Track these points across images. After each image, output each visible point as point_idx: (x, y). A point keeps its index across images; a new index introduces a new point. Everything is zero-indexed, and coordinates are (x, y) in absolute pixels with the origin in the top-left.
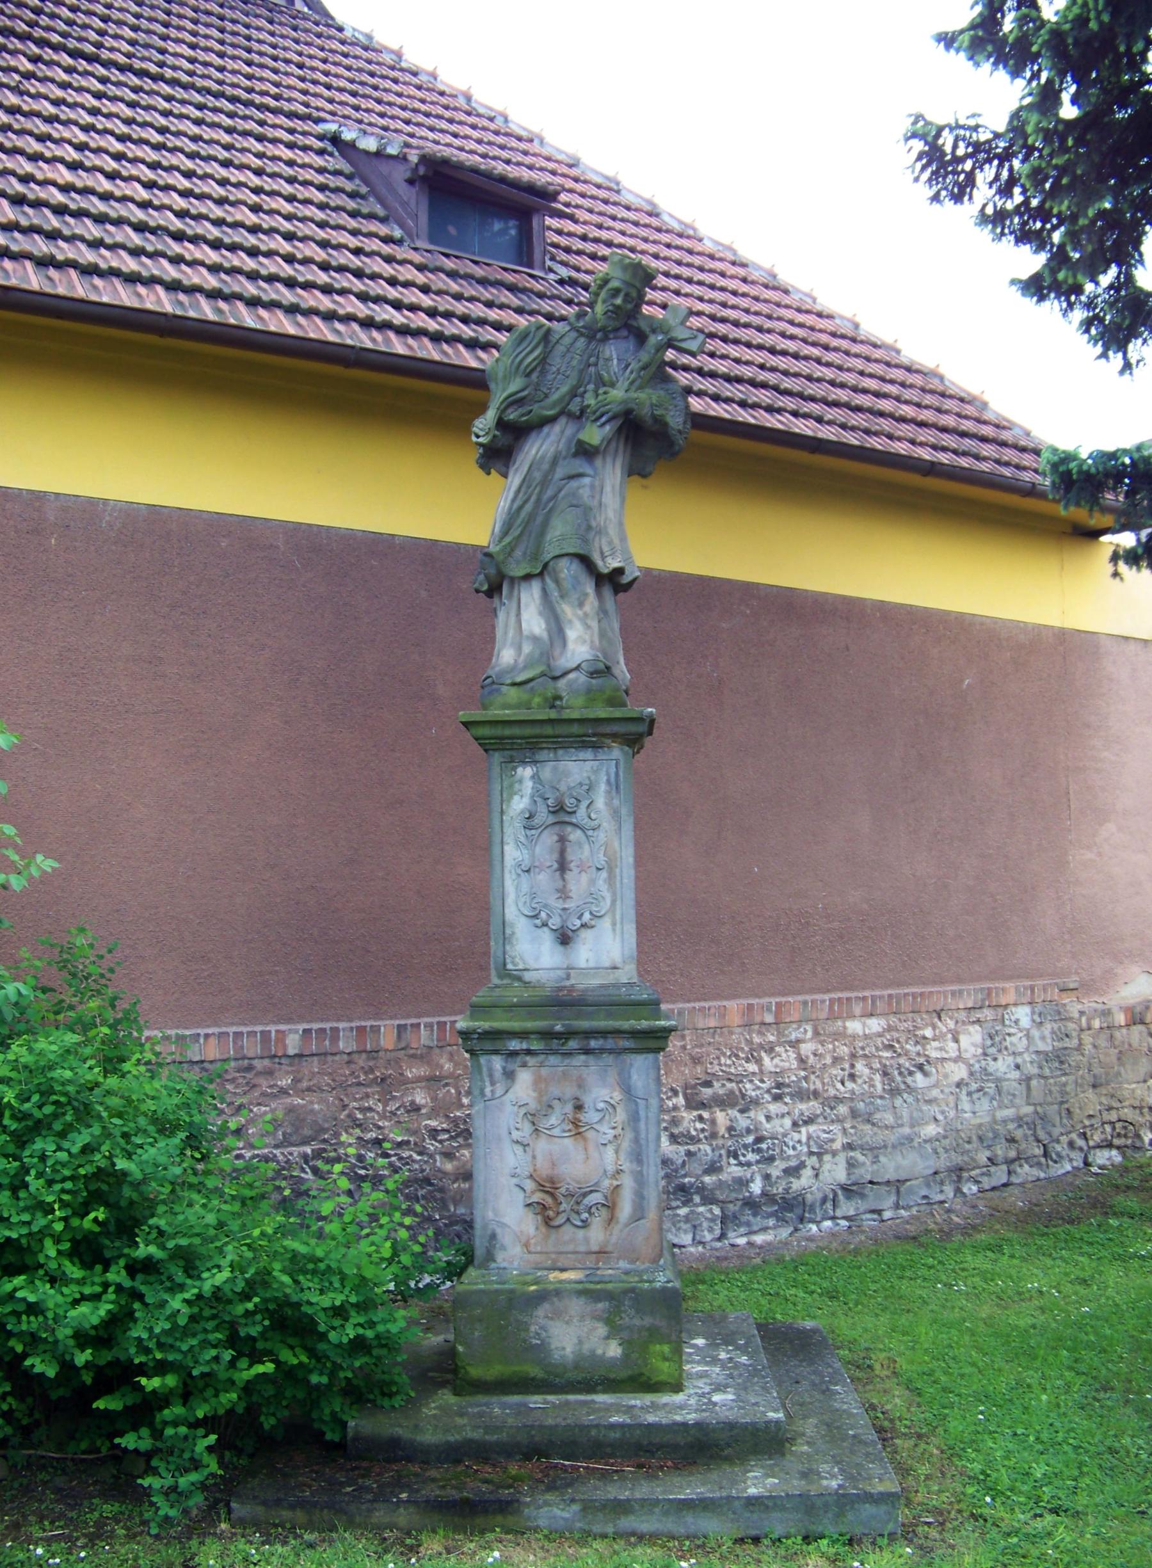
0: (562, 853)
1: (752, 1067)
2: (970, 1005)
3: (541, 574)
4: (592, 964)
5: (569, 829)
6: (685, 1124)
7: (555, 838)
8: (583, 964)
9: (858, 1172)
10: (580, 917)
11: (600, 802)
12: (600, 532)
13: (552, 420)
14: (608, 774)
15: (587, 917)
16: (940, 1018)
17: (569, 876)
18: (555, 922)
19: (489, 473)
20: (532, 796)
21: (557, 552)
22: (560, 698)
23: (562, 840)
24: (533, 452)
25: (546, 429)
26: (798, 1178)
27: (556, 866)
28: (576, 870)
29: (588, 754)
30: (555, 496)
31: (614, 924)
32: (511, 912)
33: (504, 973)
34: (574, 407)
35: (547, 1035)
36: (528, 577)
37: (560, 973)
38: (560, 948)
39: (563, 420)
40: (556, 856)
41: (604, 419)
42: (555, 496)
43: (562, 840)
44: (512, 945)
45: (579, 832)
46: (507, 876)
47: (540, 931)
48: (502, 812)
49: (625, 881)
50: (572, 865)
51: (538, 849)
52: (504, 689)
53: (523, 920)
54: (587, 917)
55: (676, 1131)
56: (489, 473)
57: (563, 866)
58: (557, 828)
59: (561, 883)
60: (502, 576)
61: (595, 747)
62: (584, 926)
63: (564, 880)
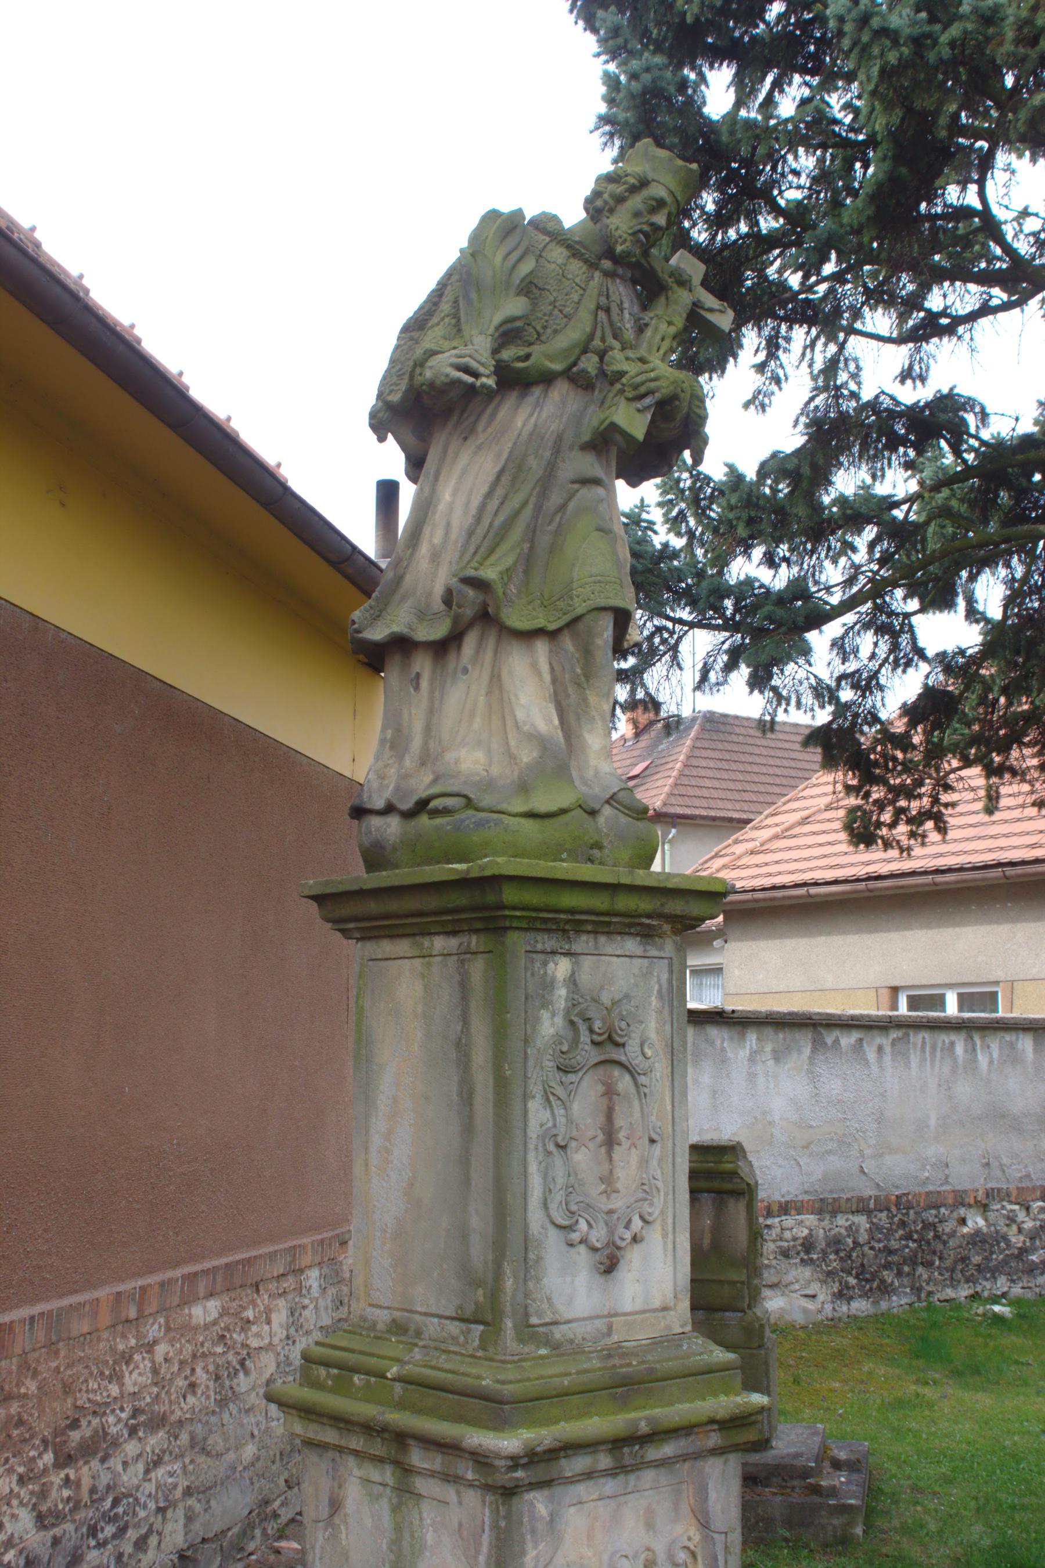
0: (610, 1115)
1: (114, 1390)
2: (281, 1271)
3: (552, 635)
4: (639, 1306)
5: (617, 1072)
6: (54, 1494)
7: (601, 1088)
8: (628, 1308)
9: (196, 1526)
10: (627, 1226)
11: (653, 1025)
12: (976, 602)
13: (547, 379)
14: (659, 981)
15: (637, 1224)
16: (258, 1291)
17: (618, 1152)
18: (598, 1236)
19: (382, 439)
20: (567, 1012)
21: (603, 602)
22: (599, 846)
23: (610, 1092)
24: (519, 424)
25: (537, 391)
26: (146, 1551)
27: (601, 1137)
28: (626, 1144)
29: (631, 945)
30: (563, 507)
31: (665, 1236)
32: (536, 1217)
33: (527, 1332)
34: (589, 364)
35: (617, 1443)
36: (529, 636)
37: (599, 1324)
38: (600, 1280)
39: (561, 389)
40: (601, 1118)
41: (648, 401)
42: (563, 507)
43: (610, 1092)
44: (538, 1280)
45: (627, 1078)
46: (531, 1157)
47: (573, 1251)
48: (526, 1041)
49: (678, 1160)
50: (621, 1135)
51: (575, 1107)
52: (507, 820)
53: (552, 1232)
54: (637, 1224)
55: (44, 1508)
56: (382, 439)
57: (610, 1141)
58: (601, 1070)
59: (606, 1166)
60: (486, 618)
61: (647, 935)
62: (635, 1239)
63: (611, 1159)
